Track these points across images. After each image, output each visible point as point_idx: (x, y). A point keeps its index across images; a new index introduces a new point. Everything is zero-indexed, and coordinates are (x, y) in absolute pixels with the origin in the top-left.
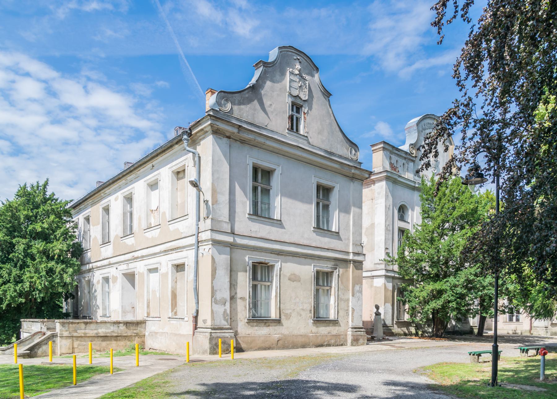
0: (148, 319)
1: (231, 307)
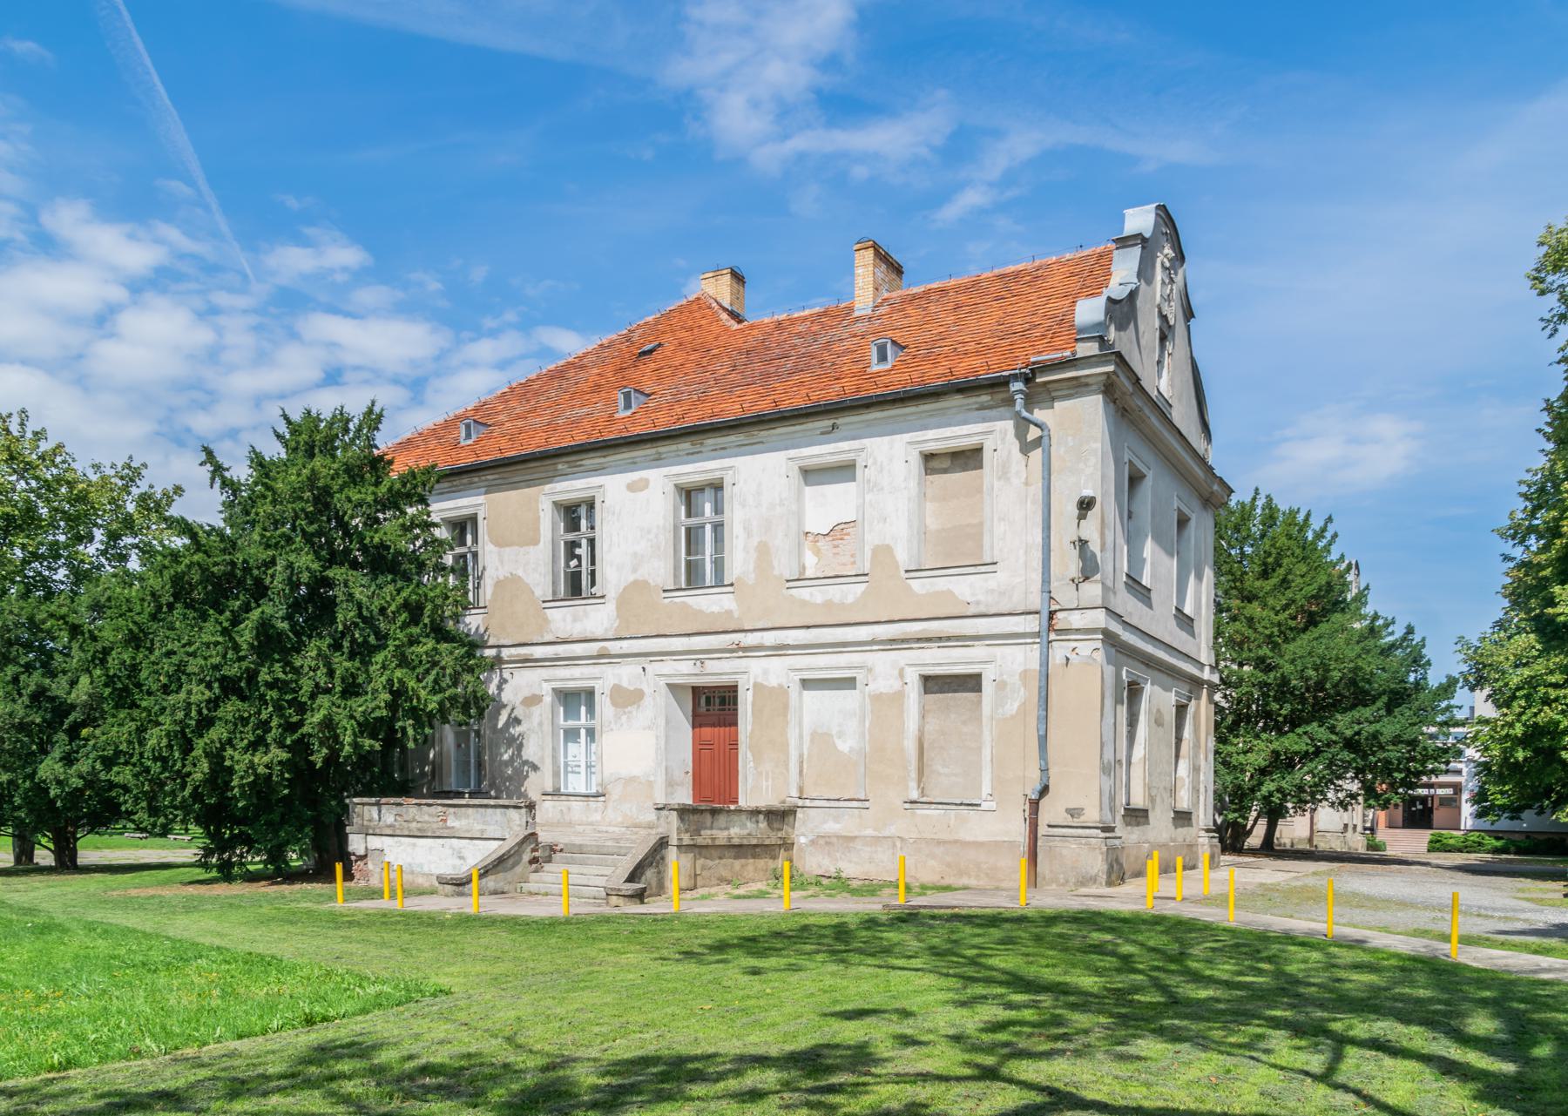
0: (800, 803)
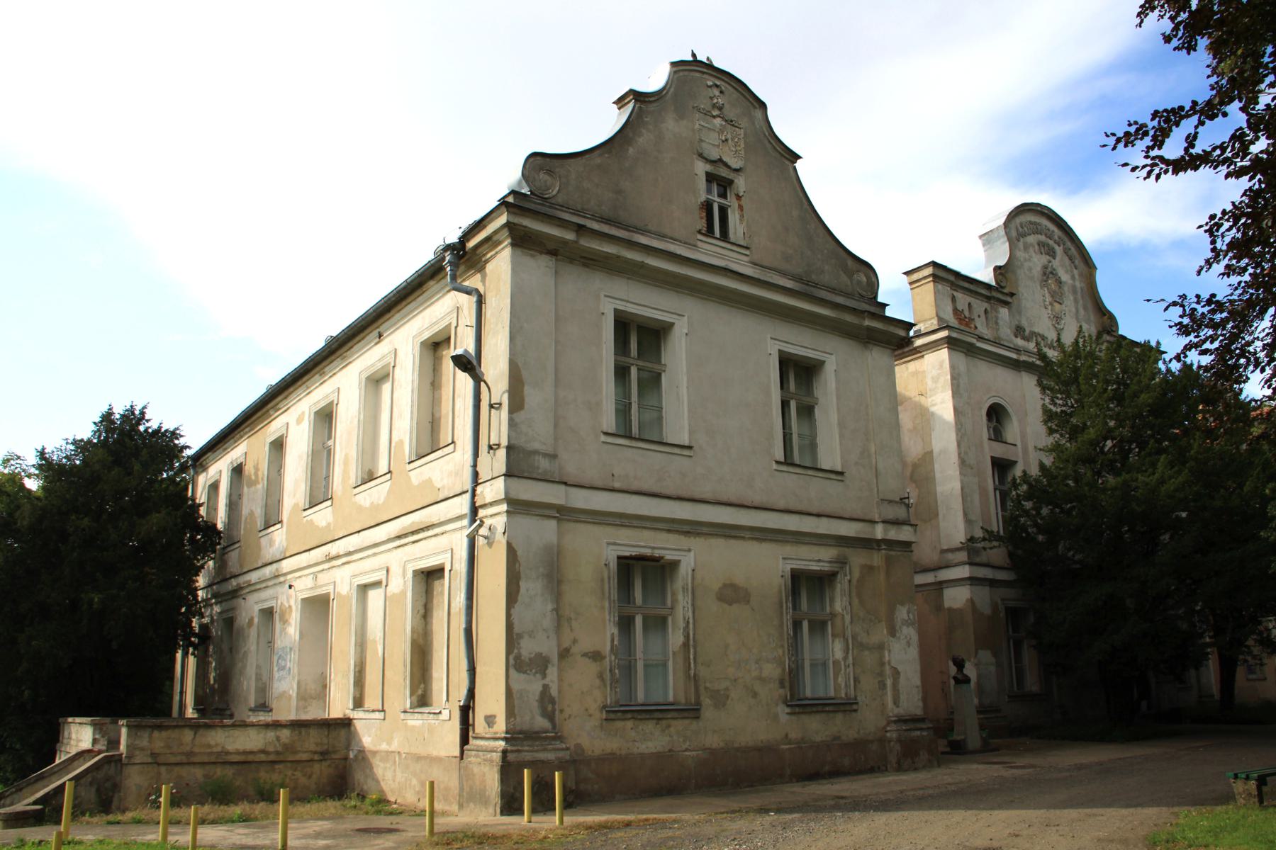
1: (560, 679)
